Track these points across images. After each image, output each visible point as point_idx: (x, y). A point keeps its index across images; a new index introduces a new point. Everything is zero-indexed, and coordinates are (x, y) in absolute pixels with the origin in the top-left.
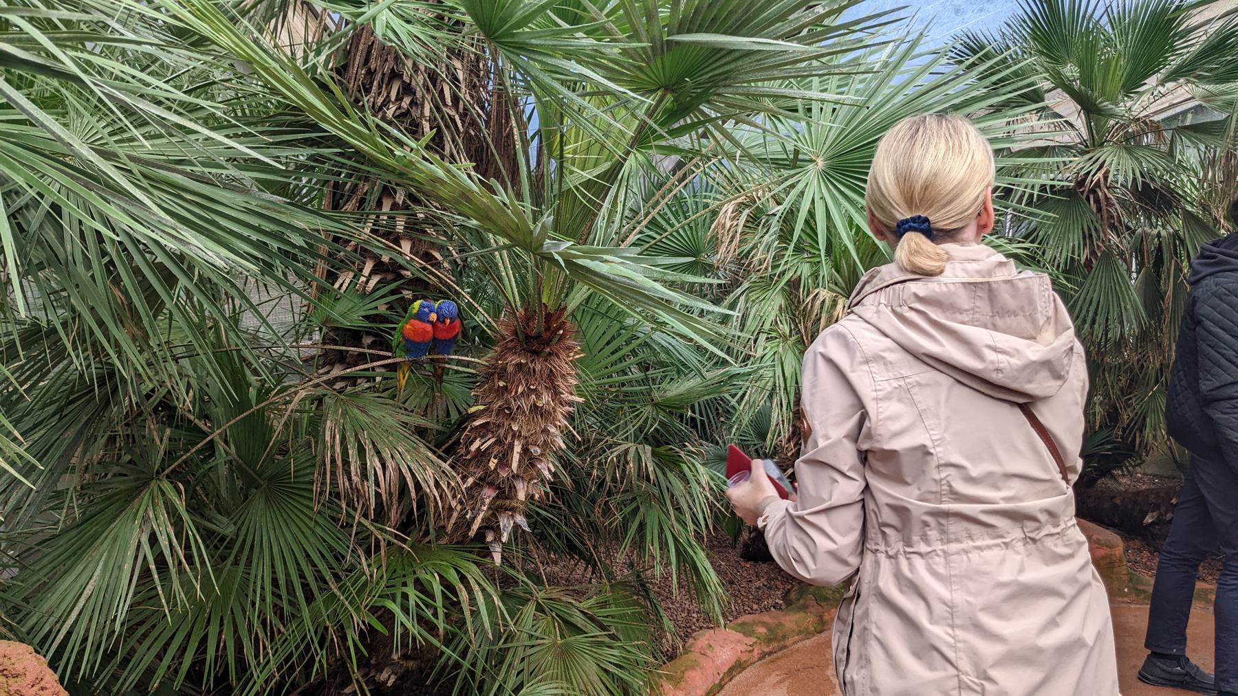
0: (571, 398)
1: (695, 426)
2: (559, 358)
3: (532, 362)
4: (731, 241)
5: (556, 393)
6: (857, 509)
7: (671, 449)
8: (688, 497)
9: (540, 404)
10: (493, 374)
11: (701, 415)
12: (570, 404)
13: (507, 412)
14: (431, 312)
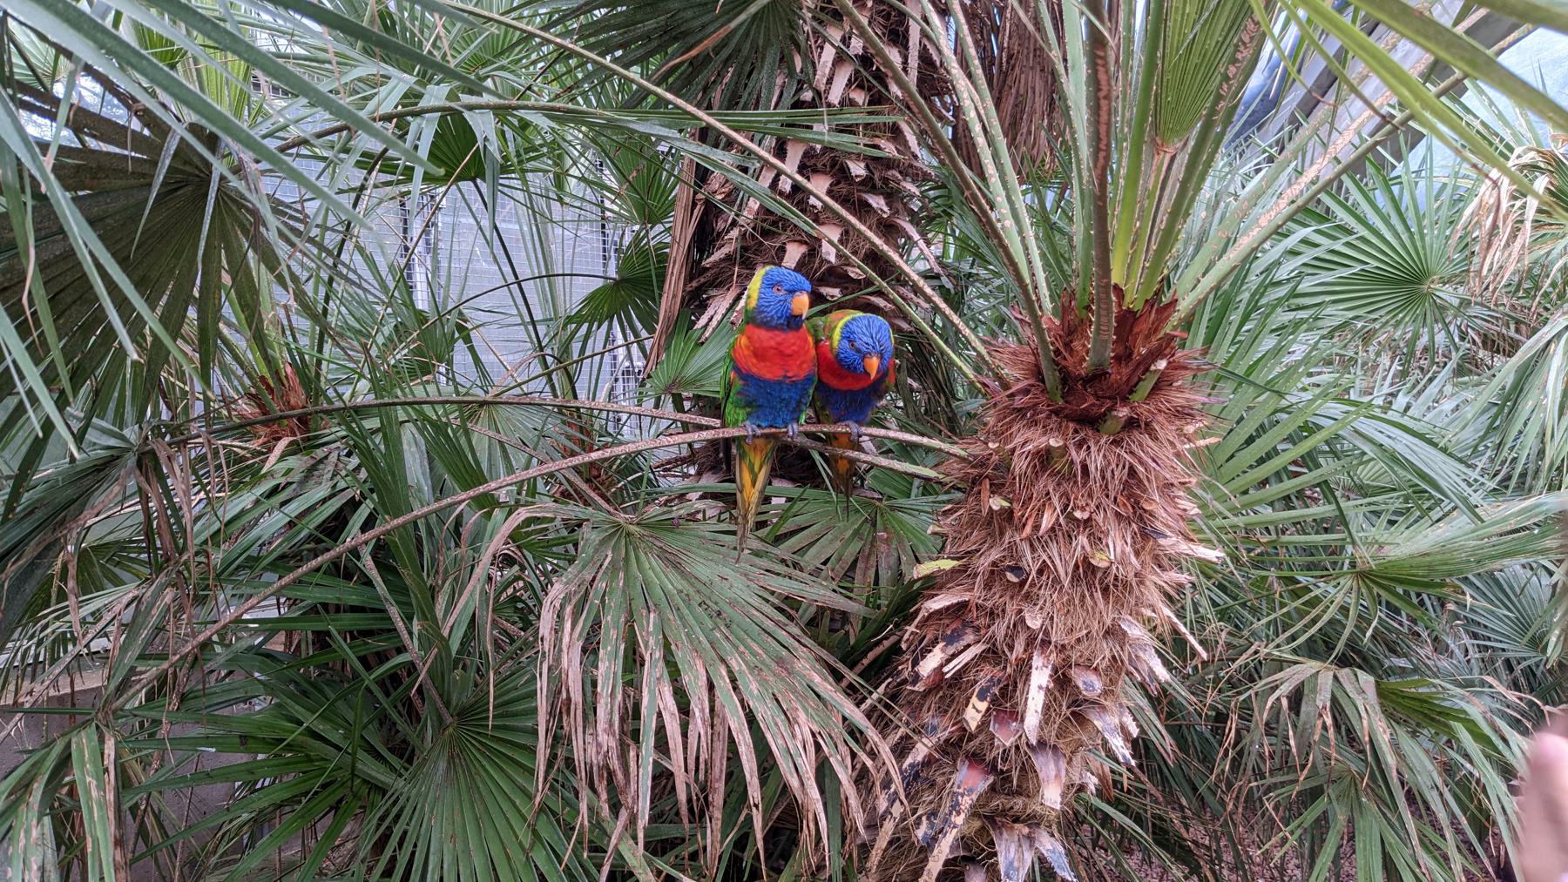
3: (1079, 445)
5: (1145, 534)
9: (1099, 560)
10: (976, 481)
13: (1011, 577)
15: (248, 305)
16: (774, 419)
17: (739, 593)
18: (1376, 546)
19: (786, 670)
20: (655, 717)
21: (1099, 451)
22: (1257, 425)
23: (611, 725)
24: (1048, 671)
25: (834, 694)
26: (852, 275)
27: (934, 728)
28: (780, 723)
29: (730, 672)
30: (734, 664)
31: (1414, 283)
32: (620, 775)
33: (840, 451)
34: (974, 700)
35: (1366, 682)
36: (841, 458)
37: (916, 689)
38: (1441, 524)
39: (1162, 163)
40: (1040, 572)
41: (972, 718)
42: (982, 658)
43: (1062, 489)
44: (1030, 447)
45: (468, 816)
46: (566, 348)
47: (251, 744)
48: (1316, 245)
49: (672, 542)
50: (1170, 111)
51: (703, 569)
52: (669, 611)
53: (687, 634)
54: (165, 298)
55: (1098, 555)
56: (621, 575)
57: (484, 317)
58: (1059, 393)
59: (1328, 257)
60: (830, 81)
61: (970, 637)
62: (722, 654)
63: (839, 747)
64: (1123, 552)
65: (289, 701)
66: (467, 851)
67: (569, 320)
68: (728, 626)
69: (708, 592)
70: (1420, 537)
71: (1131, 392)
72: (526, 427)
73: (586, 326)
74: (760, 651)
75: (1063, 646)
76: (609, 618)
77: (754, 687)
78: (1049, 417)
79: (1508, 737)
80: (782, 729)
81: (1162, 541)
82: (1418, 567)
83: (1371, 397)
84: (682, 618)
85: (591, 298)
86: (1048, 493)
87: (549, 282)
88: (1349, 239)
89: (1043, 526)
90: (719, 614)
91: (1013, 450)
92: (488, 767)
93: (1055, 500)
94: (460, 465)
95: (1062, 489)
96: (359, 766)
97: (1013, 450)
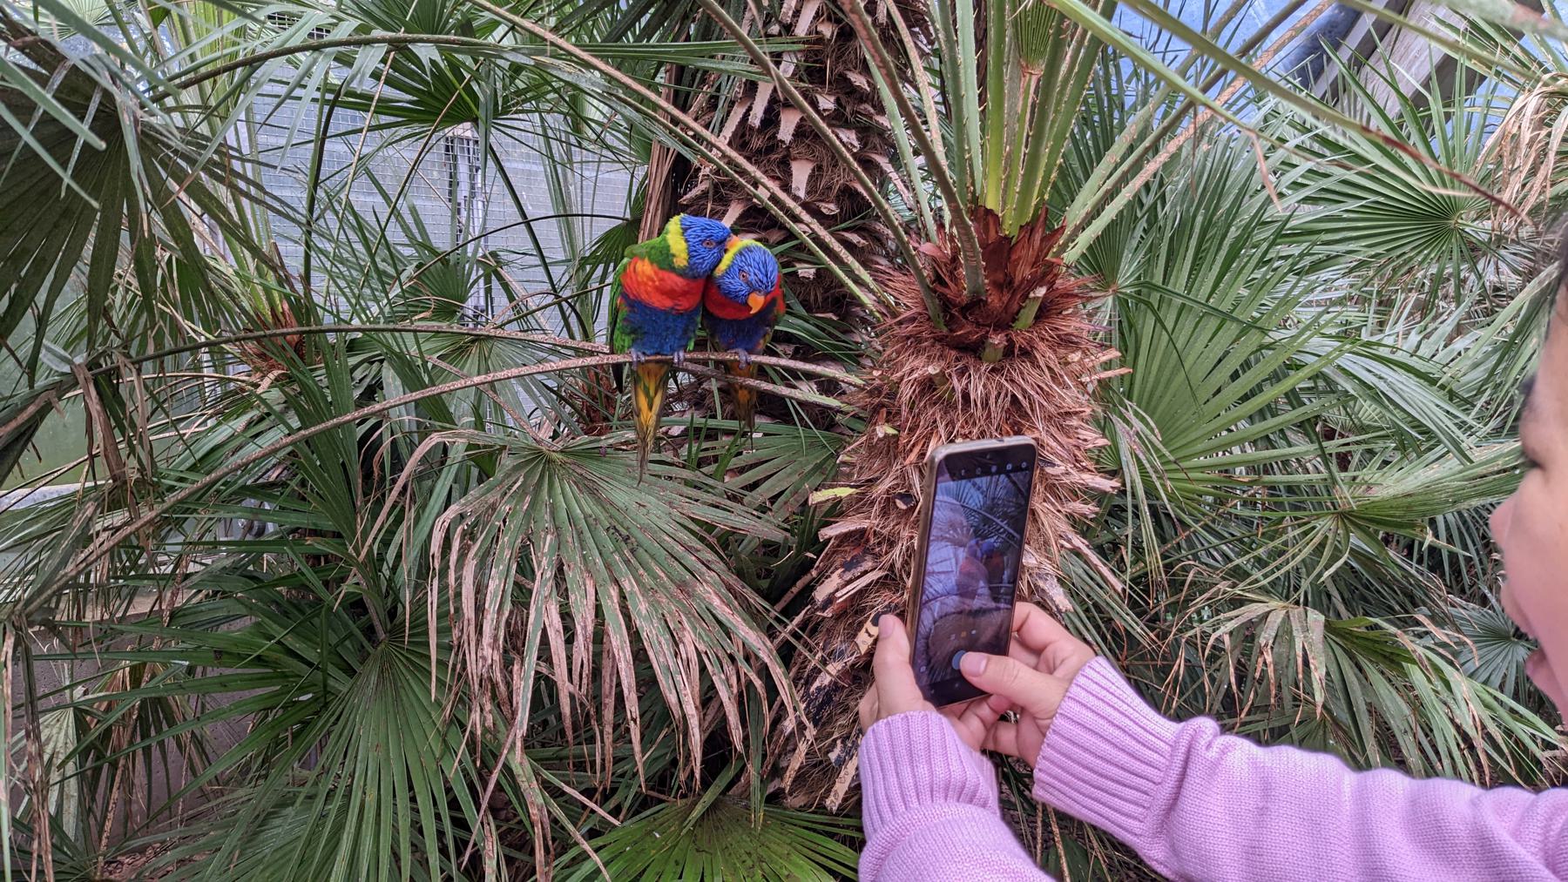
0: (1078, 478)
1: (1436, 567)
2: (1037, 366)
3: (962, 373)
4: (1533, 172)
7: (1376, 627)
8: (1421, 735)
10: (876, 410)
11: (1450, 540)
12: (1075, 493)
13: (901, 505)
15: (180, 237)
16: (661, 346)
17: (655, 519)
18: (1364, 487)
19: (688, 593)
20: (539, 633)
21: (980, 378)
22: (1241, 361)
23: (496, 638)
25: (731, 617)
26: (824, 211)
27: (842, 653)
28: (663, 642)
29: (623, 597)
30: (627, 586)
31: (1439, 218)
32: (502, 688)
33: (740, 380)
34: (868, 625)
35: (1316, 620)
36: (741, 387)
37: (825, 614)
38: (1435, 466)
39: (1029, 85)
41: (864, 642)
42: (881, 584)
43: (949, 418)
44: (915, 375)
45: (391, 726)
47: (225, 659)
48: (1326, 176)
49: (594, 470)
50: (1031, 32)
51: (621, 495)
54: (94, 229)
56: (528, 499)
59: (1338, 189)
60: (797, 13)
61: (868, 564)
63: (725, 667)
65: (267, 620)
66: (388, 759)
67: (584, 261)
68: (632, 551)
69: (620, 518)
70: (1411, 478)
71: (1014, 320)
73: (601, 266)
74: (662, 575)
77: (643, 607)
79: (1451, 680)
80: (665, 647)
81: (1049, 470)
82: (1397, 508)
83: (1382, 336)
84: (581, 541)
85: (607, 237)
86: (935, 421)
87: (567, 221)
88: (1364, 169)
90: (626, 539)
91: (902, 378)
92: (413, 684)
95: (949, 418)
96: (331, 682)
97: (902, 378)
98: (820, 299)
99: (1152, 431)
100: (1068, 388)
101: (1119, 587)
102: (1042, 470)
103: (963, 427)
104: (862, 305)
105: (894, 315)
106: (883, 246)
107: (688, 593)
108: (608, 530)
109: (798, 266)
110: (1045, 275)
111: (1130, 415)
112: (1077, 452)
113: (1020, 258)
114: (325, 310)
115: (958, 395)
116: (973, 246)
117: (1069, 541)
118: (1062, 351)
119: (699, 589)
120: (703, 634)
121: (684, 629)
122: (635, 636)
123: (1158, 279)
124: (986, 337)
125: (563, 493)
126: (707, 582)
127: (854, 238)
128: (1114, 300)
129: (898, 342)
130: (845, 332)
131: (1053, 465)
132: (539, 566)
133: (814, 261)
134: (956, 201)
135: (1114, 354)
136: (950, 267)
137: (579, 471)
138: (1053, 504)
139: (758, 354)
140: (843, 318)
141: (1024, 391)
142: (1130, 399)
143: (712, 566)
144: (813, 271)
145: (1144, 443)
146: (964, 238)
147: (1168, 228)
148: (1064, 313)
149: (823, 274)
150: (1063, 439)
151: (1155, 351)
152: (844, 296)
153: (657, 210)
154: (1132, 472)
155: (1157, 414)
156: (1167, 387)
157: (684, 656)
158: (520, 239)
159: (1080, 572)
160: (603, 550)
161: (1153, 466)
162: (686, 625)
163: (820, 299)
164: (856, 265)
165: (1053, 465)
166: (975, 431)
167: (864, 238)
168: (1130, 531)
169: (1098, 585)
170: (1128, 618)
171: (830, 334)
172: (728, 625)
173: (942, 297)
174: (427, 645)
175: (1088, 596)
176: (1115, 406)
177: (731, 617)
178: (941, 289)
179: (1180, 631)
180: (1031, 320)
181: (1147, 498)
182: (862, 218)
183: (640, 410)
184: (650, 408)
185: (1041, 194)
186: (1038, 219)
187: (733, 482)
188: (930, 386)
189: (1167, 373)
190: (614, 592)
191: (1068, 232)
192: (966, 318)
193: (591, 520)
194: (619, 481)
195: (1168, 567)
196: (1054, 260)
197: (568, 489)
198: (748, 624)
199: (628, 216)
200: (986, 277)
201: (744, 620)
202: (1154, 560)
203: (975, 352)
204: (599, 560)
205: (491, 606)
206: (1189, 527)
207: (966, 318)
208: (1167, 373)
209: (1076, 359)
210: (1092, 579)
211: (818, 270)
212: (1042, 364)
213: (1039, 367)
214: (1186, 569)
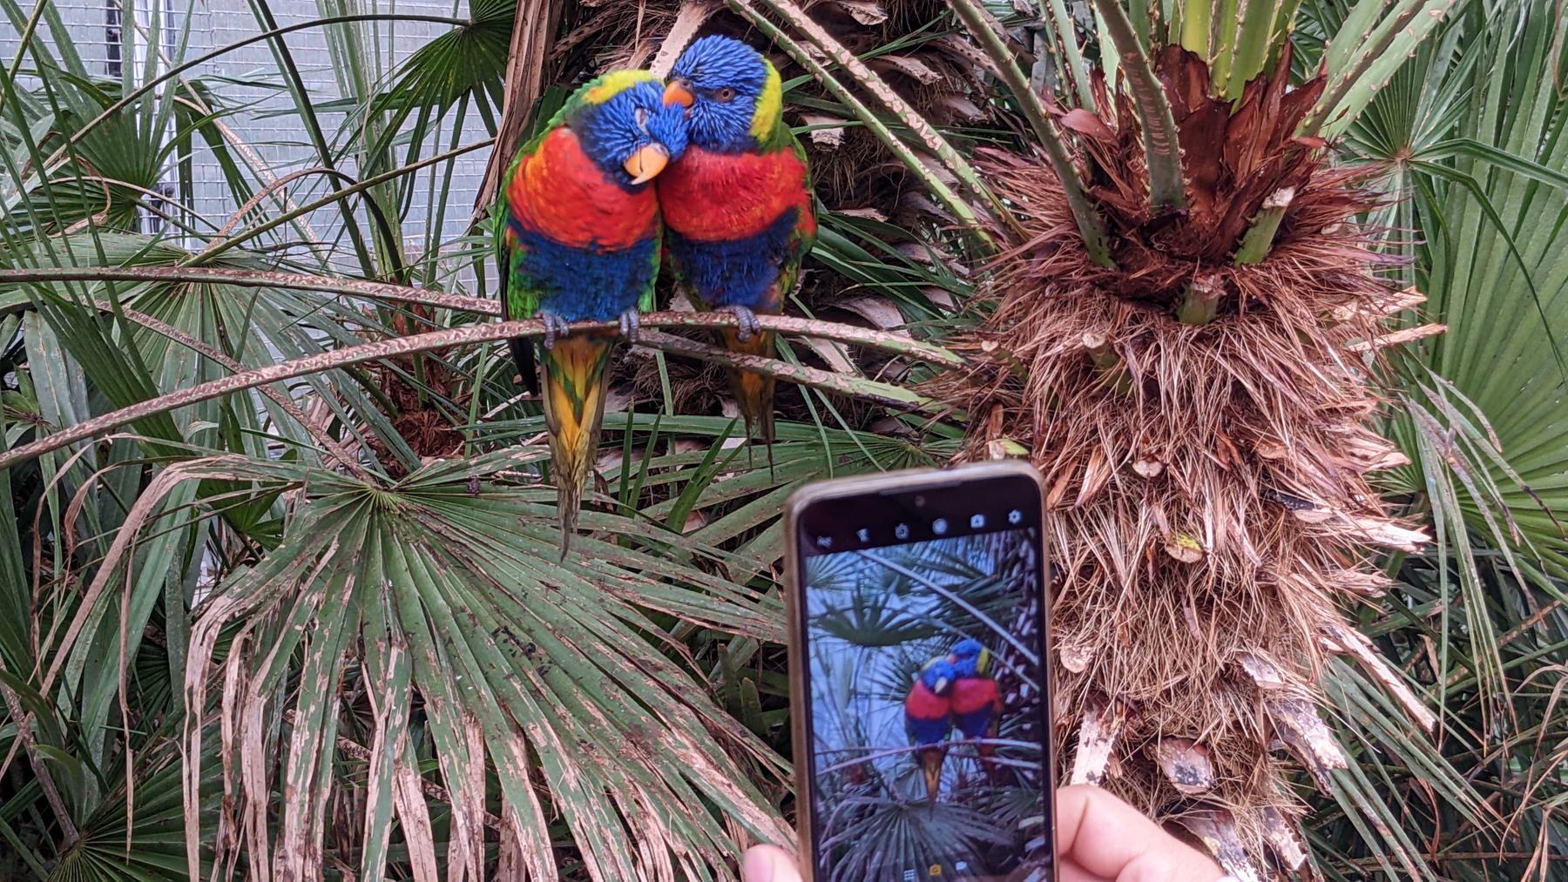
2: (1275, 326)
3: (1143, 343)
6: (335, 206)
9: (1184, 550)
10: (985, 409)
12: (1347, 553)
14: (654, 138)
17: (577, 612)
19: (645, 747)
21: (1176, 353)
23: (309, 838)
24: (1107, 748)
26: (859, 18)
28: (611, 838)
30: (538, 738)
40: (1087, 570)
44: (1058, 348)
46: (380, 156)
49: (460, 523)
52: (429, 644)
53: (458, 686)
55: (1183, 540)
57: (237, 94)
58: (1106, 251)
62: (519, 718)
64: (1230, 536)
67: (383, 101)
68: (542, 672)
71: (1236, 248)
72: (273, 311)
74: (599, 715)
75: (1138, 703)
76: (317, 657)
77: (571, 776)
78: (1090, 294)
80: (615, 848)
81: (1302, 515)
84: (452, 658)
85: (422, 60)
86: (1095, 431)
87: (347, 30)
89: (1084, 490)
93: (1107, 444)
94: (122, 386)
95: (1119, 424)
98: (851, 183)
99: (1485, 433)
100: (1330, 361)
101: (1428, 720)
102: (1289, 514)
103: (1146, 441)
104: (927, 191)
105: (1018, 240)
106: (967, 78)
107: (645, 747)
108: (495, 634)
109: (811, 121)
110: (1291, 165)
111: (1441, 401)
112: (1351, 481)
113: (1245, 138)
114: (66, 279)
115: (1138, 385)
116: (1164, 122)
117: (1337, 639)
118: (1322, 302)
119: (667, 740)
120: (679, 822)
121: (647, 814)
122: (558, 827)
123: (1486, 135)
124: (1186, 280)
125: (411, 569)
126: (678, 727)
127: (915, 67)
128: (1405, 177)
129: (1025, 289)
130: (896, 244)
131: (1309, 506)
132: (380, 705)
133: (841, 112)
134: (1136, 49)
135: (1411, 298)
136: (1119, 154)
137: (435, 526)
138: (1308, 575)
139: (774, 312)
140: (893, 217)
141: (1256, 376)
142: (1436, 367)
143: (686, 697)
144: (839, 131)
145: (1468, 452)
146: (1148, 109)
147: (1505, 38)
148: (1326, 231)
149: (857, 136)
150: (1325, 458)
151: (1483, 272)
152: (897, 175)
153: (540, 19)
154: (1445, 504)
155: (1486, 394)
156: (1506, 337)
157: (648, 863)
158: (261, 60)
159: (1353, 689)
160: (491, 672)
161: (1486, 496)
162: (650, 808)
163: (851, 183)
164: (914, 120)
165: (1309, 506)
166: (1169, 447)
167: (933, 67)
168: (1442, 606)
169: (1382, 709)
170: (1440, 772)
171: (869, 247)
172: (723, 804)
173: (1106, 208)
174: (183, 853)
175: (1365, 731)
176: (1412, 382)
177: (726, 791)
178: (1105, 195)
179: (1538, 795)
180: (1266, 247)
181: (1474, 545)
182: (931, 29)
183: (559, 424)
184: (578, 419)
185: (1282, 23)
186: (1278, 66)
187: (706, 537)
188: (1087, 370)
189: (1505, 312)
190: (517, 750)
191: (1330, 90)
192: (1151, 246)
193: (464, 617)
194: (506, 543)
195: (1516, 675)
196: (1307, 141)
197: (418, 560)
198: (756, 802)
199: (465, 13)
200: (1187, 174)
201: (748, 795)
202: (1489, 665)
203: (1167, 308)
204: (486, 692)
205: (297, 777)
206: (1552, 598)
207: (1151, 246)
208: (1505, 312)
209: (1348, 316)
210: (1370, 698)
211: (847, 129)
212: (1287, 325)
213: (1282, 331)
214: (1548, 680)
